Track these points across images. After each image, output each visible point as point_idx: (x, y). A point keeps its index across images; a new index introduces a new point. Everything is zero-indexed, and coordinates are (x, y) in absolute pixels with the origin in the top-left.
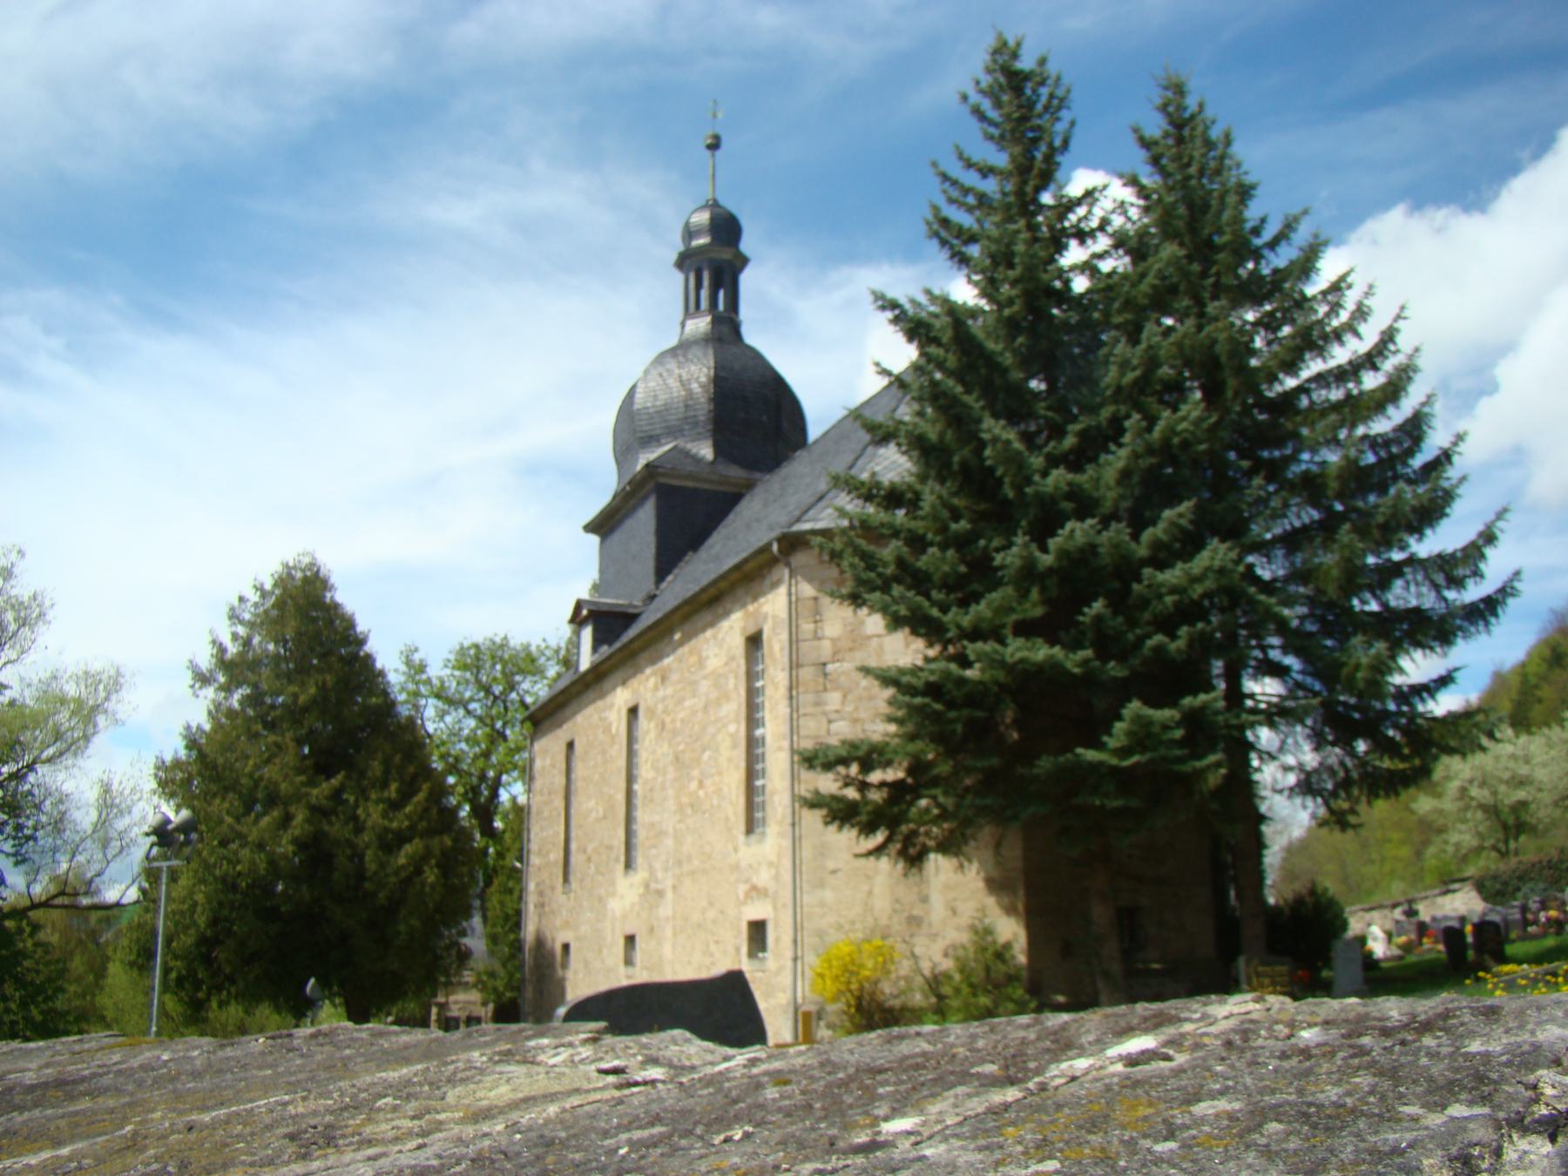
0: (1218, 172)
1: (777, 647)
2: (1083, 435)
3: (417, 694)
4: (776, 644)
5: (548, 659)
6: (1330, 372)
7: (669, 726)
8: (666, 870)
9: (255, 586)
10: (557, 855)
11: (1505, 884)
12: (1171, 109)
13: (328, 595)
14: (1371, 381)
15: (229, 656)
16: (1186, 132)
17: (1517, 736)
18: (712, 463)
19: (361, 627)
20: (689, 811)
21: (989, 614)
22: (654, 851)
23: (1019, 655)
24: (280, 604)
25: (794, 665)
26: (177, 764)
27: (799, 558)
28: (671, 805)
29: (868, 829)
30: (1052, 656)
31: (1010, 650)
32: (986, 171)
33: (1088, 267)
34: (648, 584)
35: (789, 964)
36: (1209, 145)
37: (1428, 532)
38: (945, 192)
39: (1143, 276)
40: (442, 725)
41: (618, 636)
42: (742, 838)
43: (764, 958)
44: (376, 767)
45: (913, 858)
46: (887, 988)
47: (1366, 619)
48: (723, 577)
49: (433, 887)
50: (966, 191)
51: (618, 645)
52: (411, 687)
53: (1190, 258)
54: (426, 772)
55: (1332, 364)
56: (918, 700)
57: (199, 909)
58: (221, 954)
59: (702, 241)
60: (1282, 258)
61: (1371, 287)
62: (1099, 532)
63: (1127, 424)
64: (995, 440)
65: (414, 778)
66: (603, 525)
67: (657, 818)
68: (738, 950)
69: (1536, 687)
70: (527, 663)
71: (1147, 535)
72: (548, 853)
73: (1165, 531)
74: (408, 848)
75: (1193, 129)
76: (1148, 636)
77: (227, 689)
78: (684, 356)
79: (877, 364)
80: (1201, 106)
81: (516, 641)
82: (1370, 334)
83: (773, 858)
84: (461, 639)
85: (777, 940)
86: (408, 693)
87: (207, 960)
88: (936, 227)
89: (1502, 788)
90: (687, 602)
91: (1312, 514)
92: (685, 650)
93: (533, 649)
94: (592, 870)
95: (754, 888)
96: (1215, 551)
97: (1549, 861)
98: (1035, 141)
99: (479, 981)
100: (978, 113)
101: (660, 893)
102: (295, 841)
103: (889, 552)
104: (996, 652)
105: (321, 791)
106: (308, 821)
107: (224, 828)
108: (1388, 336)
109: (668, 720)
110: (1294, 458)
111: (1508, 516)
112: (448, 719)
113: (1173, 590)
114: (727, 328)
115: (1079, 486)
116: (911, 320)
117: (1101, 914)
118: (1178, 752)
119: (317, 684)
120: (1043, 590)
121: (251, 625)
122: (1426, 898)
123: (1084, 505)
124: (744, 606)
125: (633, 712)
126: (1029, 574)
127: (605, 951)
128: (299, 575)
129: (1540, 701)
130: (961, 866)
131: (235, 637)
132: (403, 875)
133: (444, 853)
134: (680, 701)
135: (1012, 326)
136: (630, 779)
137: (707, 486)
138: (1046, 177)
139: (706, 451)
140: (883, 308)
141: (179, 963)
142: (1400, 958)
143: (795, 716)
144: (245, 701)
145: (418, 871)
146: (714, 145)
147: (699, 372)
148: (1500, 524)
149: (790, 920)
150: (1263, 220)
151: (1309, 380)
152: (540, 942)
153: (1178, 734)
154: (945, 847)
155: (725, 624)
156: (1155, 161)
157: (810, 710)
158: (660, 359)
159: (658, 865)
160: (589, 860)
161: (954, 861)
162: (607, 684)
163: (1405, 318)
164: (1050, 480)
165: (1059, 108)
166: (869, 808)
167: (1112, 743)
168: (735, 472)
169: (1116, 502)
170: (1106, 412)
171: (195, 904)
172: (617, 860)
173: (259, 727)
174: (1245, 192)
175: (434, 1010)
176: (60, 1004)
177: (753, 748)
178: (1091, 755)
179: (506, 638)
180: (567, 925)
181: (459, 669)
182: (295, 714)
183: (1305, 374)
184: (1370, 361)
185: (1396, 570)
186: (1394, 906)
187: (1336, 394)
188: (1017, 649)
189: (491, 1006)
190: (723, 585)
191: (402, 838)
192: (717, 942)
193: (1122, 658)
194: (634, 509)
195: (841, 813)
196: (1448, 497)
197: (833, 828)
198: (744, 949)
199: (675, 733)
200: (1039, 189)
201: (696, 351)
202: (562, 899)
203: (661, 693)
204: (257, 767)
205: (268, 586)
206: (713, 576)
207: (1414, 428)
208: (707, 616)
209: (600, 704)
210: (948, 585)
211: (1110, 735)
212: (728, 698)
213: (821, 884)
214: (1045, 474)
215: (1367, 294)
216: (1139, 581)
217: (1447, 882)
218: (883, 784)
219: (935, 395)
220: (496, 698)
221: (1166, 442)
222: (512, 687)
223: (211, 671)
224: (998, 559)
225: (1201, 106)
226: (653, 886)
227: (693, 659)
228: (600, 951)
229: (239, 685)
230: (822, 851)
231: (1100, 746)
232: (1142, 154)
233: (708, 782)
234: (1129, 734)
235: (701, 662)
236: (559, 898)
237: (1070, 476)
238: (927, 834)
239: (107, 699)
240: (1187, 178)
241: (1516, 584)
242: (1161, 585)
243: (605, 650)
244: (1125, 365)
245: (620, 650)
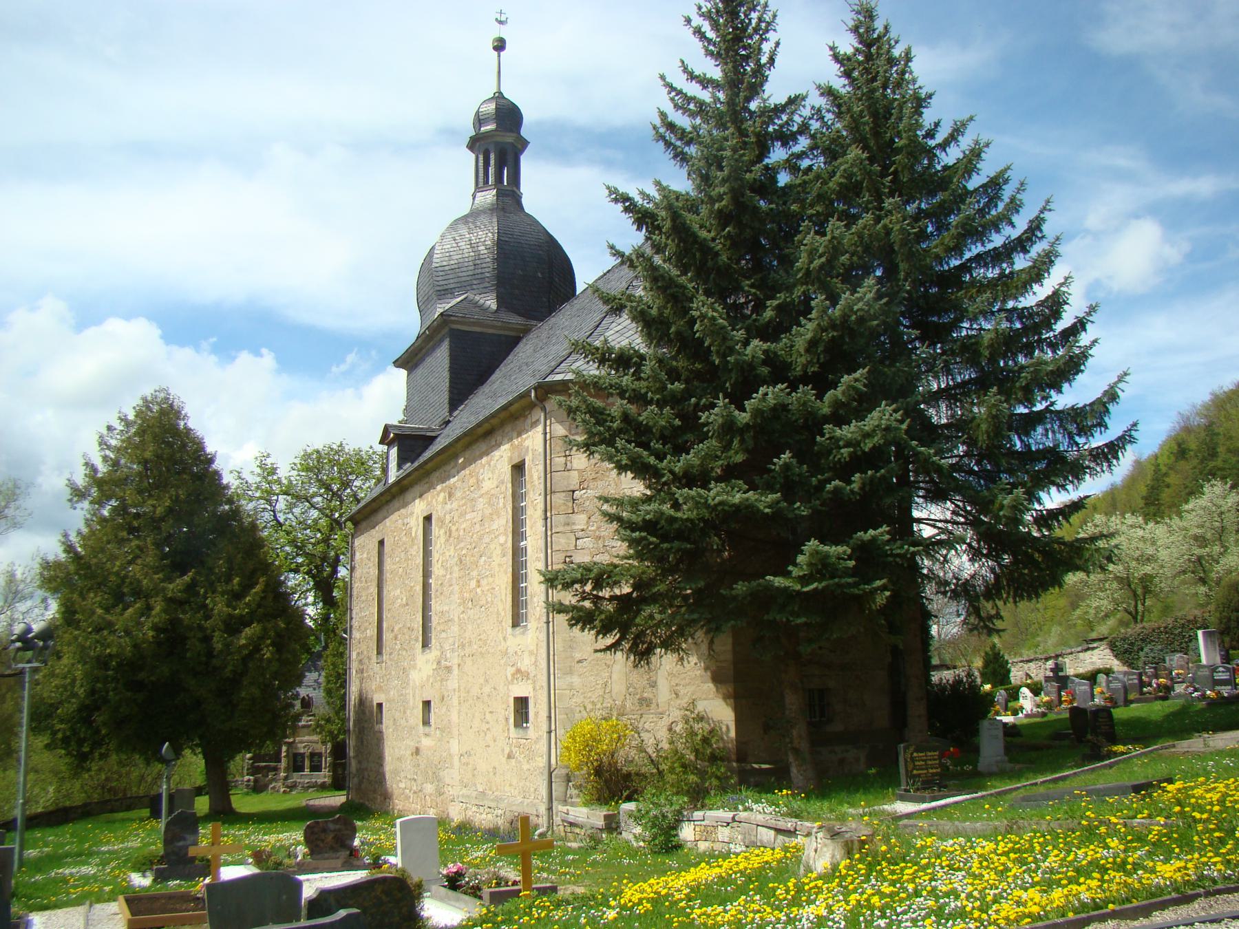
0: (899, 85)
1: (535, 476)
2: (780, 309)
3: (270, 492)
4: (534, 472)
7: (454, 534)
9: (120, 418)
10: (372, 632)
11: (1132, 644)
12: (861, 31)
13: (182, 423)
15: (100, 475)
16: (873, 50)
18: (496, 311)
19: (210, 449)
21: (697, 462)
22: (444, 635)
24: (141, 432)
25: (548, 492)
26: (58, 565)
27: (553, 402)
28: (456, 597)
29: (605, 630)
31: (712, 493)
32: (705, 82)
35: (545, 735)
37: (1065, 386)
40: (290, 516)
41: (419, 455)
42: (510, 629)
43: (527, 727)
44: (221, 565)
45: (642, 653)
46: (620, 757)
48: (493, 416)
49: (269, 661)
50: (689, 99)
51: (416, 464)
52: (265, 486)
54: (265, 568)
55: (990, 246)
57: (78, 683)
58: (99, 718)
59: (490, 127)
60: (951, 156)
62: (789, 394)
63: (813, 303)
66: (410, 360)
67: (446, 608)
68: (507, 719)
69: (1166, 475)
70: (360, 464)
71: (830, 395)
72: (366, 629)
73: (843, 393)
74: (248, 631)
75: (879, 48)
76: (829, 481)
77: (100, 502)
78: (473, 223)
79: (612, 247)
80: (886, 28)
81: (350, 447)
82: (1021, 223)
83: (533, 648)
85: (537, 714)
86: (262, 492)
87: (88, 721)
88: (662, 130)
89: (1134, 564)
90: (465, 435)
91: (969, 374)
92: (467, 471)
94: (398, 647)
95: (518, 671)
96: (883, 412)
97: (1165, 628)
98: (746, 58)
100: (698, 32)
101: (449, 669)
102: (155, 628)
105: (176, 586)
106: (165, 611)
107: (95, 618)
109: (454, 528)
110: (955, 325)
111: (1127, 378)
112: (297, 511)
114: (509, 197)
116: (638, 212)
117: (792, 702)
118: (850, 580)
119: (170, 498)
120: (742, 441)
122: (1072, 653)
123: (779, 371)
124: (511, 439)
125: (428, 519)
126: (729, 429)
127: (408, 712)
128: (156, 408)
129: (1168, 486)
130: (682, 659)
131: (105, 458)
132: (246, 652)
134: (463, 515)
135: (724, 218)
136: (427, 574)
137: (491, 331)
139: (491, 303)
140: (616, 201)
141: (63, 726)
143: (549, 533)
144: (114, 510)
145: (257, 649)
146: (500, 46)
147: (486, 236)
150: (937, 125)
151: (970, 260)
152: (362, 702)
153: (852, 563)
154: (667, 644)
155: (496, 454)
159: (447, 647)
160: (396, 638)
162: (409, 496)
163: (1050, 210)
164: (749, 350)
165: (767, 31)
167: (796, 572)
168: (515, 320)
169: (805, 367)
170: (798, 291)
172: (417, 640)
173: (124, 534)
174: (920, 102)
175: (284, 748)
177: (518, 554)
178: (779, 581)
179: (341, 445)
180: (380, 688)
181: (303, 471)
183: (967, 255)
184: (1021, 244)
186: (1047, 659)
187: (992, 273)
188: (717, 493)
189: (329, 745)
190: (495, 421)
191: (245, 622)
192: (491, 712)
193: (806, 500)
194: (433, 349)
195: (582, 619)
198: (512, 720)
200: (749, 99)
201: (484, 219)
202: (376, 667)
203: (448, 507)
204: (123, 567)
205: (131, 417)
206: (487, 413)
208: (483, 446)
209: (403, 511)
211: (795, 565)
213: (570, 672)
214: (746, 343)
215: (1018, 191)
216: (822, 435)
217: (1088, 644)
218: (612, 598)
219: (656, 278)
220: (334, 494)
221: (845, 317)
222: (346, 484)
223: (85, 487)
224: (704, 417)
226: (443, 663)
227: (472, 481)
228: (405, 712)
229: (109, 498)
230: (571, 645)
231: (787, 574)
232: (835, 68)
233: (484, 582)
234: (810, 564)
236: (374, 667)
237: (765, 346)
240: (873, 91)
243: (408, 467)
244: (812, 254)
245: (420, 466)
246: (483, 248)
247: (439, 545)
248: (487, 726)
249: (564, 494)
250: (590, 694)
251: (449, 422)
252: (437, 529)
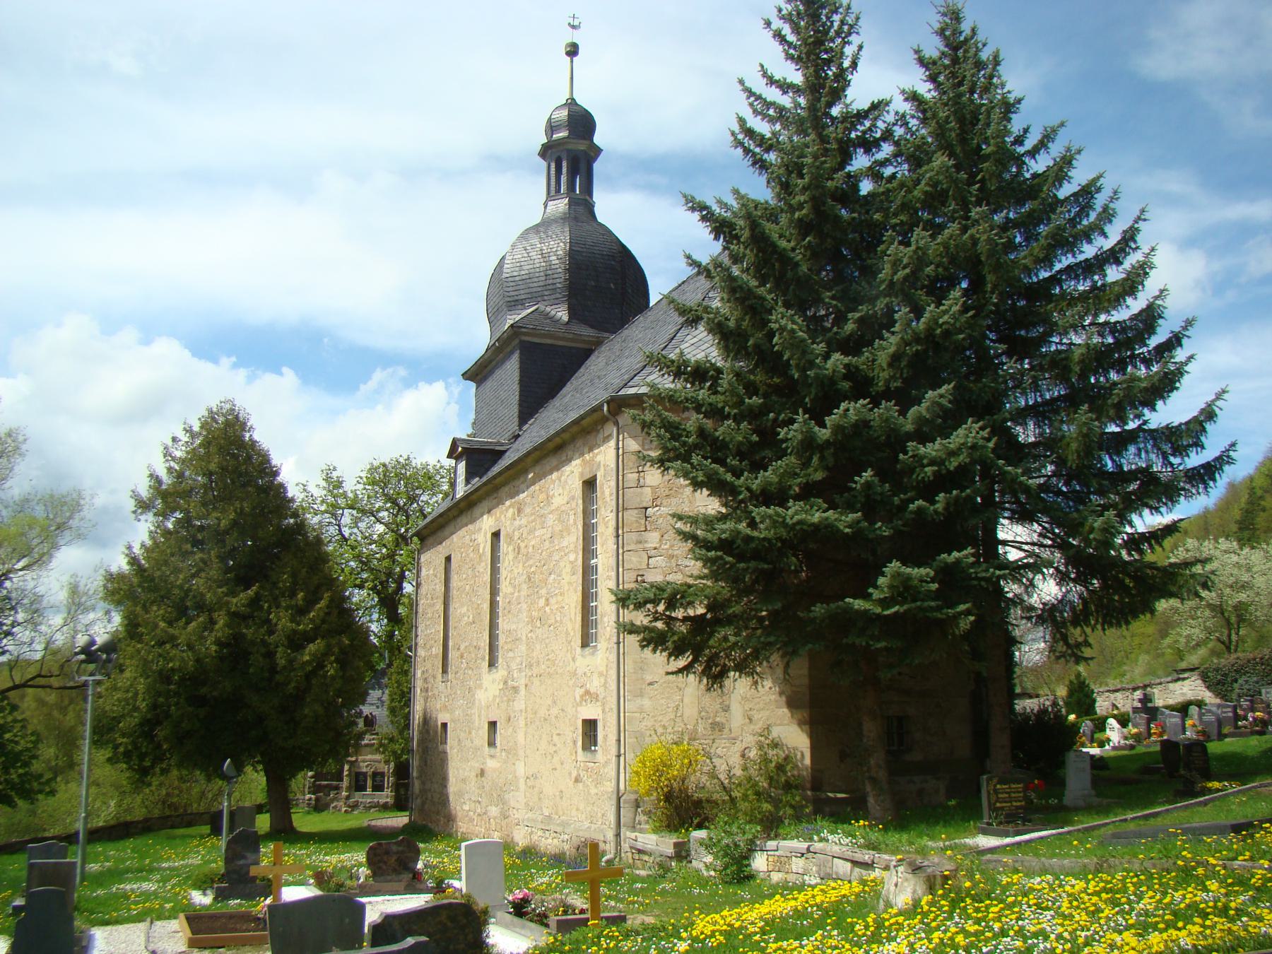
0: (986, 89)
1: (607, 492)
2: (861, 321)
4: (606, 489)
5: (443, 477)
6: (1078, 265)
7: (523, 551)
8: (520, 670)
9: (185, 429)
10: (437, 650)
11: (1225, 675)
12: (947, 33)
13: (247, 435)
14: (1114, 274)
16: (960, 53)
17: (1241, 549)
18: (567, 323)
20: (538, 624)
22: (511, 654)
23: (797, 518)
24: (207, 444)
25: (620, 509)
27: (626, 417)
29: (677, 652)
30: (827, 519)
31: (790, 512)
32: (785, 87)
33: (874, 173)
34: (514, 426)
36: (979, 65)
38: (751, 105)
39: (917, 182)
41: (488, 470)
42: (579, 650)
45: (715, 676)
48: (563, 430)
49: (333, 678)
50: (769, 105)
51: (485, 479)
52: (330, 499)
53: (958, 167)
54: (330, 583)
55: (1081, 258)
56: (712, 554)
57: (140, 697)
59: (563, 134)
60: (1039, 165)
61: (1115, 192)
62: (871, 410)
63: (896, 316)
64: (782, 329)
65: (318, 587)
66: (479, 373)
68: (575, 742)
72: (431, 647)
73: (928, 409)
74: (312, 647)
75: (966, 51)
76: (912, 501)
79: (688, 257)
80: (973, 30)
83: (603, 669)
84: (371, 460)
85: (606, 737)
87: (149, 736)
88: (740, 137)
89: (1228, 591)
91: (1058, 391)
92: (537, 487)
93: (430, 468)
95: (587, 692)
99: (381, 745)
100: (779, 36)
102: (218, 642)
103: (692, 421)
104: (778, 515)
105: (240, 600)
106: (227, 625)
107: (158, 631)
108: (1129, 238)
109: (522, 545)
111: (1225, 396)
113: (932, 462)
115: (857, 368)
116: (716, 221)
119: (235, 511)
120: (822, 458)
121: (182, 461)
122: (1161, 684)
123: (860, 385)
125: (496, 535)
126: (809, 445)
128: (221, 419)
129: (1264, 510)
130: (756, 683)
131: (170, 470)
133: (343, 651)
134: (532, 531)
135: (804, 228)
136: (494, 592)
138: (837, 94)
139: (562, 314)
140: (693, 209)
142: (1132, 747)
143: (621, 551)
145: (321, 666)
146: (573, 51)
147: (557, 246)
148: (1219, 403)
149: (615, 722)
150: (1026, 131)
151: (1060, 272)
152: (426, 721)
154: (741, 667)
155: (567, 469)
156: (933, 79)
158: (525, 235)
159: (514, 666)
160: (462, 657)
161: (749, 679)
162: (477, 511)
163: (1145, 220)
164: (830, 364)
165: (849, 34)
166: (676, 638)
167: (876, 594)
168: (587, 332)
169: (887, 382)
170: (881, 304)
171: (136, 694)
174: (1009, 108)
175: (346, 767)
176: (36, 767)
178: (858, 604)
182: (220, 536)
183: (1058, 267)
184: (1114, 256)
185: (1131, 437)
186: (1134, 689)
188: (795, 512)
189: (392, 765)
190: (566, 436)
191: (309, 638)
192: (559, 734)
193: (888, 520)
194: (503, 362)
195: (653, 640)
196: (1179, 372)
197: (648, 652)
199: (527, 556)
200: (830, 105)
201: (556, 229)
202: (441, 686)
203: (517, 523)
204: (187, 580)
205: (196, 428)
207: (1150, 317)
208: (553, 461)
209: (470, 527)
210: (741, 455)
211: (876, 587)
213: (641, 694)
214: (827, 357)
215: (1112, 199)
216: (905, 453)
218: (685, 619)
219: (734, 289)
221: (930, 330)
223: (149, 499)
224: (782, 433)
225: (973, 30)
226: (510, 683)
227: (542, 497)
230: (641, 667)
231: (867, 597)
232: (921, 73)
233: (553, 601)
234: (891, 587)
235: (549, 498)
237: (847, 360)
238: (728, 656)
239: (70, 518)
240: (960, 95)
241: (1231, 453)
242: (924, 457)
243: (476, 481)
244: (896, 264)
248: (554, 749)
249: (636, 511)
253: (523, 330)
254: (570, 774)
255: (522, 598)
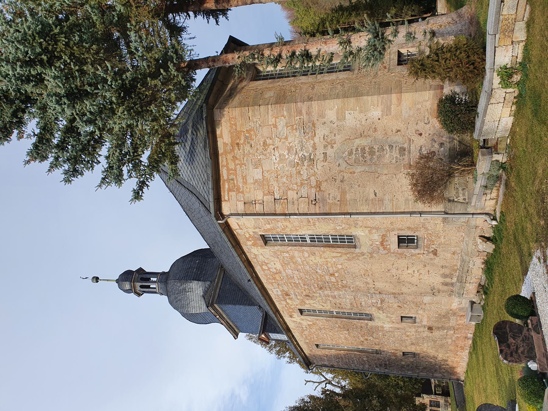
42: (357, 250)
47: (540, 20)
95: (382, 244)
146: (96, 279)
157: (296, 206)
212: (292, 258)
226: (379, 305)
246: (181, 287)
247: (315, 305)
248: (416, 272)
249: (276, 205)
250: (397, 188)
251: (259, 306)
252: (306, 306)
253: (210, 302)
254: (431, 259)
255: (332, 294)
